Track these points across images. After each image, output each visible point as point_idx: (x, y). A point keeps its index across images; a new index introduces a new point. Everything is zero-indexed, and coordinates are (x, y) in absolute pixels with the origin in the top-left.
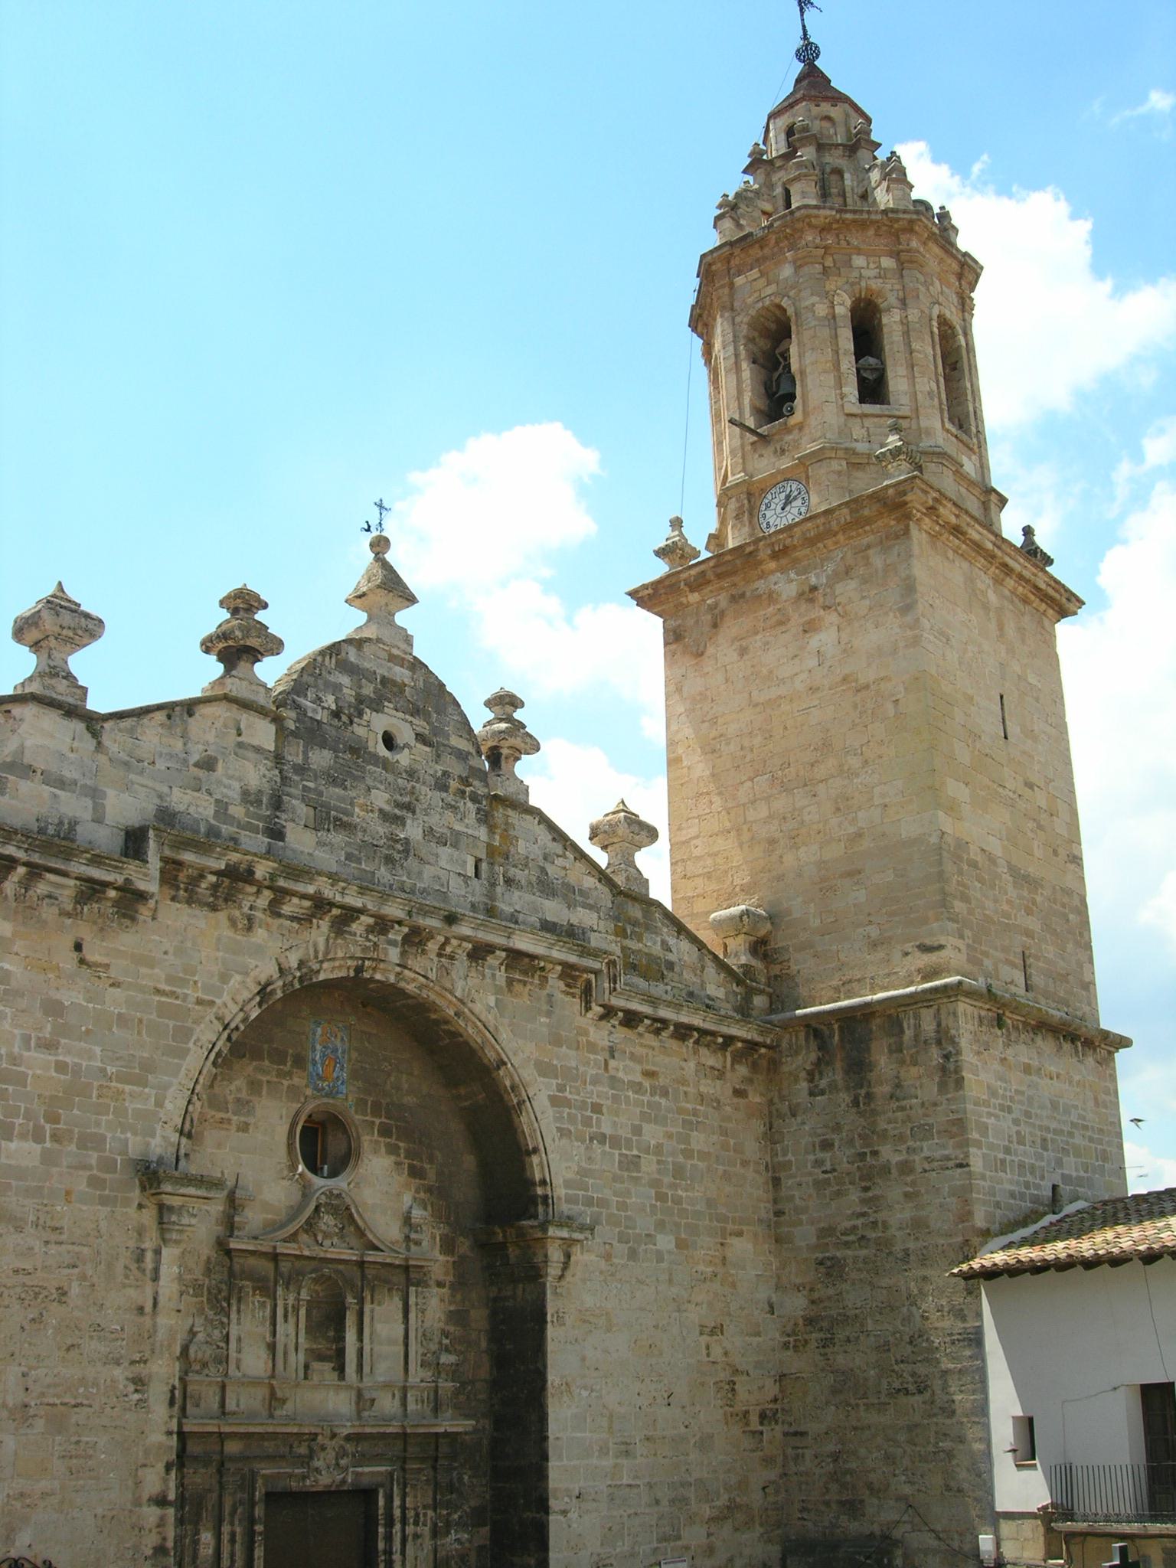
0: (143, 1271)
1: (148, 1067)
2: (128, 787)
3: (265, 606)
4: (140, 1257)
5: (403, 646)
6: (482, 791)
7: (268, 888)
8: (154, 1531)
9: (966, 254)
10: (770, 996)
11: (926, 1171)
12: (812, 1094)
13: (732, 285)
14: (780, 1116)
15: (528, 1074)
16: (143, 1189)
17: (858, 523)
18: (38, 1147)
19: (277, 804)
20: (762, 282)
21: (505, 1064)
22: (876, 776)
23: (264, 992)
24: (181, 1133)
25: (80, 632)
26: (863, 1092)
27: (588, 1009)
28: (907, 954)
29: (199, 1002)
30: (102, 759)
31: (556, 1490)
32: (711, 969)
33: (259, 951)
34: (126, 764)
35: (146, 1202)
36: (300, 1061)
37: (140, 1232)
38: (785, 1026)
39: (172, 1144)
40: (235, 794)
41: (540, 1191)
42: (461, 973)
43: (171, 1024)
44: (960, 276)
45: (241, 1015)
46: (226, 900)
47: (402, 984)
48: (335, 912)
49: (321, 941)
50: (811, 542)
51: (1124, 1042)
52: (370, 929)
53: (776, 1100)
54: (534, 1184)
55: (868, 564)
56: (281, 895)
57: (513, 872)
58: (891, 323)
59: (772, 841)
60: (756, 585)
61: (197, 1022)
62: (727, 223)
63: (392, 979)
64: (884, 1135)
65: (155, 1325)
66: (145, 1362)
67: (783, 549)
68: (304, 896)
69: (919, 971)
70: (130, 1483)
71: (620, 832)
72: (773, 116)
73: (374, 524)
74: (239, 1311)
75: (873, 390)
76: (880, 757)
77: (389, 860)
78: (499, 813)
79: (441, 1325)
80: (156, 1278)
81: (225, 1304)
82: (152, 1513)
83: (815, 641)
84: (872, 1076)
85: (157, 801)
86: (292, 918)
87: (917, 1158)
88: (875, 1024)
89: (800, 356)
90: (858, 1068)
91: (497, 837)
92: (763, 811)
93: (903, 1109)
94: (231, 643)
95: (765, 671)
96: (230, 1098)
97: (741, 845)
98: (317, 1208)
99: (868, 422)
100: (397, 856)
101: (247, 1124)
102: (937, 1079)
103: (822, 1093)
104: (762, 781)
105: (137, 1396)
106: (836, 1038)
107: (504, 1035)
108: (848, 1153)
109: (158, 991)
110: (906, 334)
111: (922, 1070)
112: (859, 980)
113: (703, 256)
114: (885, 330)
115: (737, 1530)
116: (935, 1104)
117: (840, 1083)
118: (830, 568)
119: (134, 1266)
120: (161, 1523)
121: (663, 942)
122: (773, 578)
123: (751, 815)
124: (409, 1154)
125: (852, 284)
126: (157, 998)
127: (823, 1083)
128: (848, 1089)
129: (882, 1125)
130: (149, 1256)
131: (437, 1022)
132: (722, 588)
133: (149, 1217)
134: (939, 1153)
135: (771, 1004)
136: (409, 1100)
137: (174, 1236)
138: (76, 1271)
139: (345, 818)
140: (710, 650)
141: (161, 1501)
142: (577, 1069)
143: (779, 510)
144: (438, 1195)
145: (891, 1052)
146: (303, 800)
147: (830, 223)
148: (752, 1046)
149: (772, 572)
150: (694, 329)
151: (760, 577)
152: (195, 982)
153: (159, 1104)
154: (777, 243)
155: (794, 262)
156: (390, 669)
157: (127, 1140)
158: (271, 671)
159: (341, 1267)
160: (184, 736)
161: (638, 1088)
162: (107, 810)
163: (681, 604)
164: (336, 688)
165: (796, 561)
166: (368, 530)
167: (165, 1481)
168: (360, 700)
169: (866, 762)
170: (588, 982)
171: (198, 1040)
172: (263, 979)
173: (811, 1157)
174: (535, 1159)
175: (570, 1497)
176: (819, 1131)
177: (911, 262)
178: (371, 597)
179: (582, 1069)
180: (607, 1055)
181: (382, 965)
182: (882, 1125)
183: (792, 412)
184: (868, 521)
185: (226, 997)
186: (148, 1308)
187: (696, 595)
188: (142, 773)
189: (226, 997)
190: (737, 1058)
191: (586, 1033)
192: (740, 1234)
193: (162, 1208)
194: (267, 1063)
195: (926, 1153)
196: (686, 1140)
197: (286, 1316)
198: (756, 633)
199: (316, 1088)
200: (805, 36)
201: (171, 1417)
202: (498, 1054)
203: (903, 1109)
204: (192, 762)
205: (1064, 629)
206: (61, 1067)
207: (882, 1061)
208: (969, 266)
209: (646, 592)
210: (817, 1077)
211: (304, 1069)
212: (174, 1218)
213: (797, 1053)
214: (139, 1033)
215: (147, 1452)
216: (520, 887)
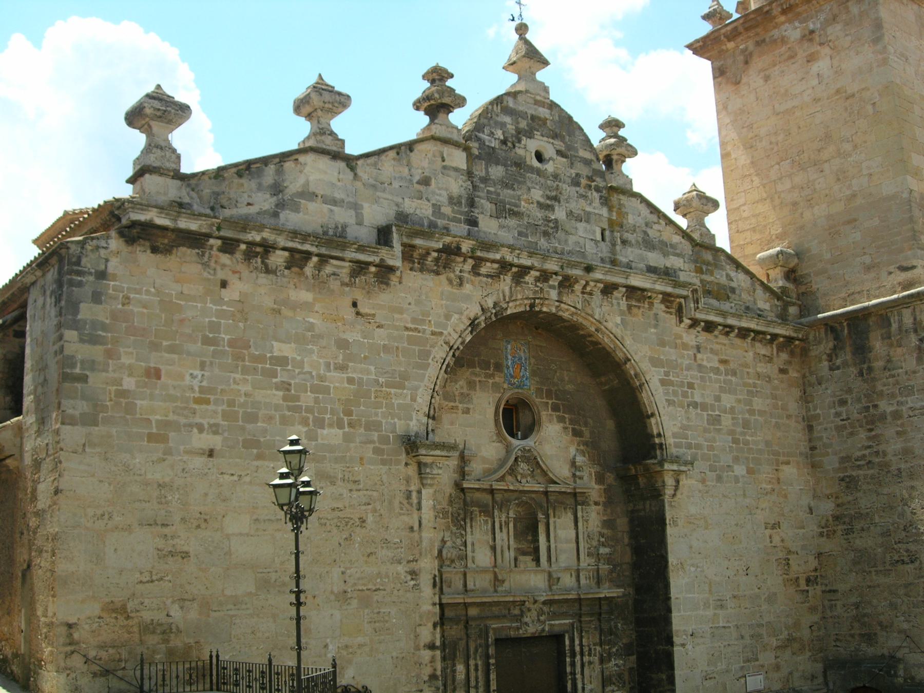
0: (411, 505)
1: (405, 377)
2: (376, 201)
3: (452, 76)
4: (409, 497)
5: (543, 94)
7: (470, 257)
8: (429, 665)
12: (831, 369)
14: (811, 385)
15: (645, 366)
16: (408, 453)
18: (340, 432)
19: (472, 203)
21: (629, 360)
23: (473, 324)
24: (429, 417)
25: (336, 105)
26: (865, 366)
27: (681, 321)
29: (433, 333)
30: (358, 184)
31: (677, 631)
32: (759, 291)
33: (467, 298)
35: (410, 462)
36: (498, 367)
37: (408, 480)
38: (811, 325)
39: (423, 424)
40: (444, 199)
41: (657, 441)
42: (598, 303)
43: (417, 348)
46: (444, 268)
47: (560, 313)
48: (514, 269)
49: (507, 289)
52: (537, 279)
53: (807, 374)
54: (653, 436)
55: (848, 12)
57: (627, 236)
59: (795, 204)
60: (772, 33)
61: (433, 346)
63: (554, 310)
64: (881, 394)
65: (421, 537)
66: (416, 561)
68: (493, 261)
69: (899, 284)
70: (412, 636)
71: (694, 205)
74: (471, 527)
76: (865, 142)
77: (546, 234)
78: (615, 198)
79: (599, 529)
80: (419, 508)
81: (462, 523)
82: (427, 654)
83: (815, 67)
84: (871, 355)
86: (487, 276)
88: (872, 321)
90: (862, 350)
91: (614, 214)
92: (788, 185)
93: (893, 376)
94: (432, 102)
95: (782, 91)
96: (457, 393)
97: (774, 208)
98: (516, 459)
100: (551, 231)
101: (468, 409)
102: (915, 355)
103: (838, 368)
104: (786, 164)
105: (412, 583)
106: (846, 331)
107: (628, 342)
108: (857, 407)
109: (407, 329)
112: (859, 292)
115: (794, 654)
116: (914, 372)
118: (822, 17)
119: (405, 502)
120: (433, 660)
122: (784, 27)
123: (780, 187)
124: (572, 422)
126: (406, 333)
128: (855, 365)
130: (414, 495)
131: (584, 336)
132: (749, 37)
133: (412, 470)
136: (569, 387)
137: (429, 481)
138: (370, 507)
139: (516, 209)
140: (745, 80)
141: (431, 647)
142: (676, 361)
144: (592, 446)
145: (883, 339)
146: (488, 200)
149: (783, 23)
151: (775, 27)
152: (430, 321)
153: (414, 399)
156: (536, 110)
157: (395, 423)
158: (460, 118)
159: (533, 496)
160: (409, 164)
161: (717, 371)
163: (723, 50)
164: (503, 125)
165: (799, 14)
166: (513, 20)
167: (433, 634)
168: (519, 132)
170: (680, 305)
172: (472, 316)
173: (833, 411)
174: (653, 420)
175: (686, 635)
176: (837, 393)
179: (679, 361)
180: (695, 351)
181: (546, 302)
185: (450, 329)
186: (416, 527)
188: (384, 191)
189: (450, 329)
191: (681, 337)
192: (788, 463)
193: (420, 465)
194: (478, 369)
195: (910, 405)
197: (501, 528)
198: (775, 65)
201: (435, 594)
203: (893, 376)
204: (415, 181)
206: (350, 381)
207: (878, 345)
210: (834, 358)
211: (502, 371)
212: (428, 470)
213: (820, 343)
214: (397, 356)
215: (421, 617)
216: (631, 245)
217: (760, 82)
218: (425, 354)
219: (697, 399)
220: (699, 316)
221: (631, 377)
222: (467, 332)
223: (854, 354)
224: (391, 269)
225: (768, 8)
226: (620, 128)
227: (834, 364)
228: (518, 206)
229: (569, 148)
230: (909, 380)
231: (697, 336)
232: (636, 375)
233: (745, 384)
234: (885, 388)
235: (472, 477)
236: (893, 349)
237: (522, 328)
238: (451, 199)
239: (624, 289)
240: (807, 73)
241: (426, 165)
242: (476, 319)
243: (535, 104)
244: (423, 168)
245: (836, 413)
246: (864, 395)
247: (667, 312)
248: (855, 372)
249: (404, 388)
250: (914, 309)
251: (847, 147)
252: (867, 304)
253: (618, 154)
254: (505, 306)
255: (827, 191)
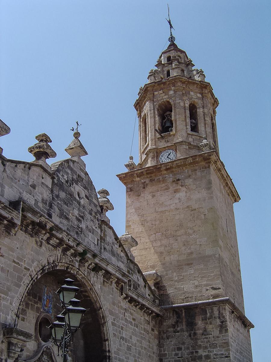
2: (11, 187)
3: (51, 142)
5: (84, 167)
6: (100, 218)
7: (48, 233)
9: (216, 99)
10: (159, 300)
11: (215, 358)
13: (154, 94)
15: (107, 313)
16: (4, 335)
17: (194, 163)
19: (51, 206)
20: (164, 94)
22: (198, 236)
25: (3, 130)
27: (122, 294)
28: (208, 290)
29: (25, 268)
30: (5, 174)
32: (147, 289)
34: (12, 179)
35: (4, 340)
38: (166, 310)
39: (13, 319)
40: (40, 199)
43: (17, 274)
44: (213, 105)
45: (37, 276)
46: (35, 234)
48: (65, 246)
49: (59, 255)
50: (178, 166)
51: (253, 327)
52: (72, 255)
54: (106, 351)
55: (196, 174)
56: (52, 236)
57: (106, 246)
58: (200, 111)
59: (161, 253)
62: (152, 77)
64: (200, 346)
67: (169, 167)
68: (57, 238)
69: (212, 295)
71: (129, 241)
72: (146, 93)
73: (75, 128)
75: (194, 128)
77: (77, 233)
78: (103, 226)
83: (178, 195)
84: (196, 327)
85: (19, 194)
87: (211, 354)
89: (175, 116)
90: (191, 325)
91: (103, 234)
92: (159, 244)
93: (207, 338)
94: (41, 150)
98: (42, 353)
99: (193, 137)
100: (79, 233)
101: (24, 318)
103: (178, 332)
106: (184, 314)
107: (102, 299)
108: (187, 352)
109: (14, 262)
110: (204, 115)
111: (213, 326)
112: (191, 297)
113: (146, 85)
114: (198, 113)
116: (218, 337)
117: (185, 329)
121: (138, 278)
125: (190, 99)
126: (14, 264)
127: (179, 329)
128: (187, 331)
129: (199, 343)
133: (4, 346)
134: (220, 353)
135: (160, 303)
137: (12, 355)
139: (67, 216)
140: (142, 195)
143: (166, 157)
145: (202, 320)
146: (57, 207)
147: (185, 82)
148: (157, 315)
150: (136, 107)
153: (11, 304)
154: (169, 84)
155: (174, 90)
156: (80, 172)
158: (50, 162)
160: (28, 174)
161: (131, 323)
162: (5, 192)
163: (133, 181)
164: (67, 174)
166: (73, 130)
168: (73, 180)
169: (194, 231)
170: (122, 286)
171: (24, 282)
173: (174, 353)
174: (107, 343)
177: (205, 96)
178: (75, 149)
181: (74, 268)
182: (199, 343)
183: (172, 130)
184: (197, 162)
185: (33, 269)
187: (139, 178)
188: (16, 183)
190: (153, 318)
191: (120, 303)
193: (10, 344)
194: (31, 297)
195: (215, 352)
196: (141, 343)
198: (158, 191)
199: (44, 309)
200: (171, 35)
202: (100, 305)
203: (207, 338)
204: (30, 184)
205: (235, 205)
207: (200, 323)
208: (216, 102)
209: (123, 176)
211: (41, 302)
212: (13, 348)
213: (170, 319)
216: (107, 251)
217: (150, 197)
218: (20, 279)
219: (124, 336)
220: (130, 294)
221: (100, 318)
222: (40, 272)
223: (187, 326)
224: (14, 225)
225: (159, 166)
226: (107, 195)
227: (176, 330)
228: (69, 215)
229: (90, 196)
230: (214, 340)
231: (126, 304)
232: (103, 317)
233: (141, 333)
234: (202, 344)
235: (22, 359)
236: (207, 325)
237: (53, 280)
238: (43, 200)
239: (104, 271)
240: (174, 197)
241: (35, 179)
242: (44, 267)
243: (80, 170)
244: (34, 179)
245: (176, 354)
246: (191, 346)
247: (117, 289)
248: (187, 334)
249: (7, 295)
250: (219, 307)
251: (190, 231)
252: (196, 302)
253: (106, 207)
254: (57, 264)
255: (179, 250)
